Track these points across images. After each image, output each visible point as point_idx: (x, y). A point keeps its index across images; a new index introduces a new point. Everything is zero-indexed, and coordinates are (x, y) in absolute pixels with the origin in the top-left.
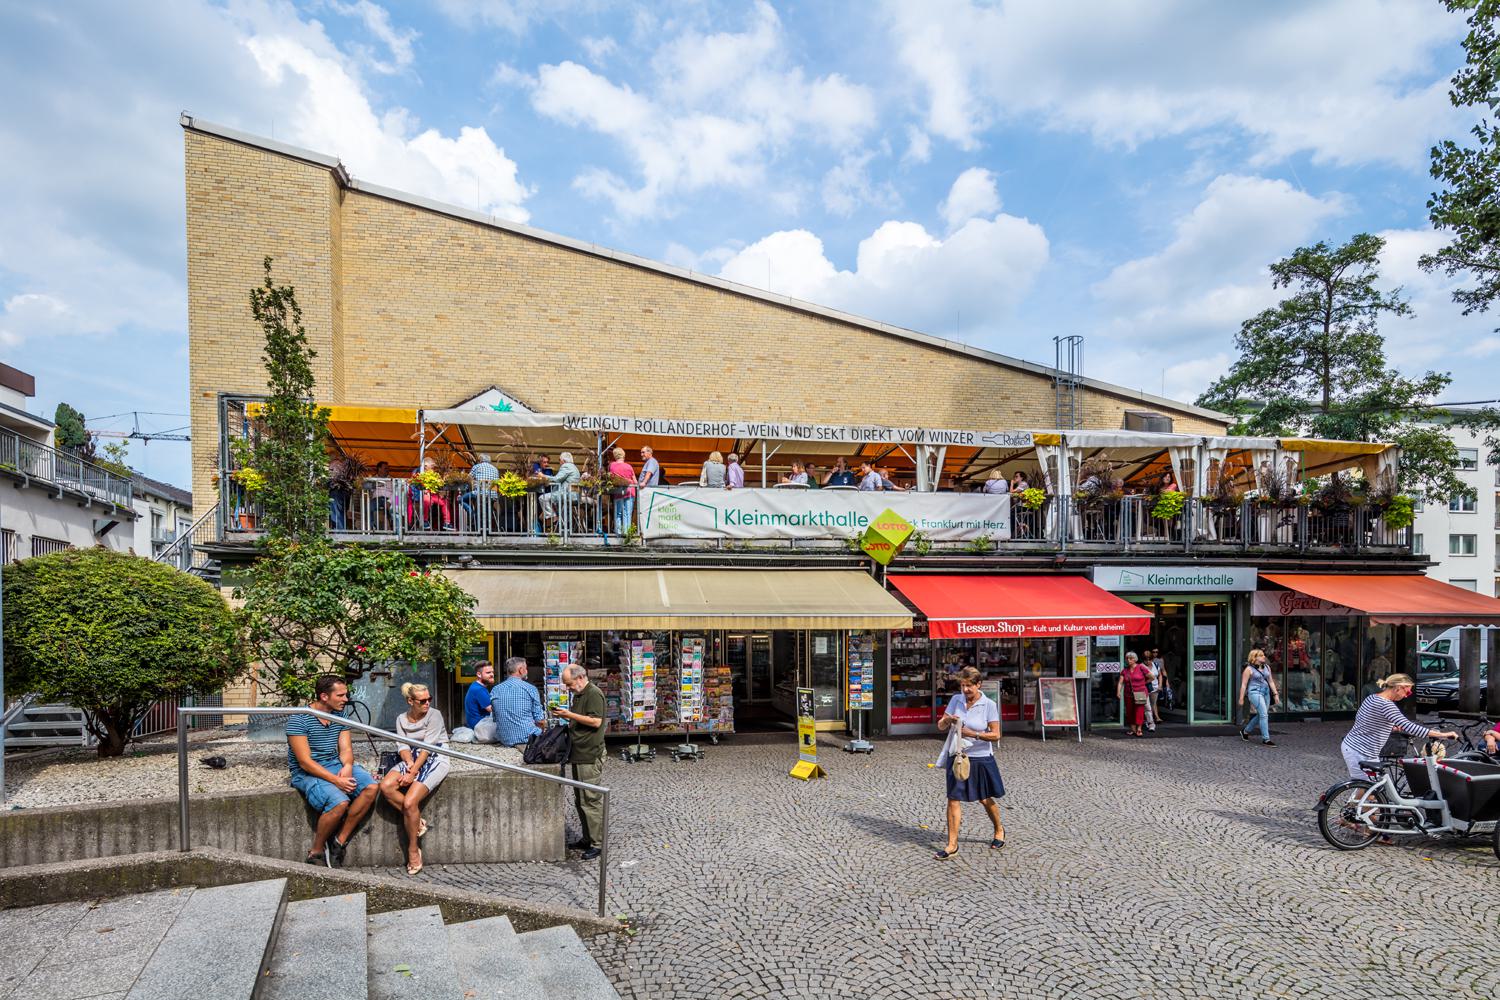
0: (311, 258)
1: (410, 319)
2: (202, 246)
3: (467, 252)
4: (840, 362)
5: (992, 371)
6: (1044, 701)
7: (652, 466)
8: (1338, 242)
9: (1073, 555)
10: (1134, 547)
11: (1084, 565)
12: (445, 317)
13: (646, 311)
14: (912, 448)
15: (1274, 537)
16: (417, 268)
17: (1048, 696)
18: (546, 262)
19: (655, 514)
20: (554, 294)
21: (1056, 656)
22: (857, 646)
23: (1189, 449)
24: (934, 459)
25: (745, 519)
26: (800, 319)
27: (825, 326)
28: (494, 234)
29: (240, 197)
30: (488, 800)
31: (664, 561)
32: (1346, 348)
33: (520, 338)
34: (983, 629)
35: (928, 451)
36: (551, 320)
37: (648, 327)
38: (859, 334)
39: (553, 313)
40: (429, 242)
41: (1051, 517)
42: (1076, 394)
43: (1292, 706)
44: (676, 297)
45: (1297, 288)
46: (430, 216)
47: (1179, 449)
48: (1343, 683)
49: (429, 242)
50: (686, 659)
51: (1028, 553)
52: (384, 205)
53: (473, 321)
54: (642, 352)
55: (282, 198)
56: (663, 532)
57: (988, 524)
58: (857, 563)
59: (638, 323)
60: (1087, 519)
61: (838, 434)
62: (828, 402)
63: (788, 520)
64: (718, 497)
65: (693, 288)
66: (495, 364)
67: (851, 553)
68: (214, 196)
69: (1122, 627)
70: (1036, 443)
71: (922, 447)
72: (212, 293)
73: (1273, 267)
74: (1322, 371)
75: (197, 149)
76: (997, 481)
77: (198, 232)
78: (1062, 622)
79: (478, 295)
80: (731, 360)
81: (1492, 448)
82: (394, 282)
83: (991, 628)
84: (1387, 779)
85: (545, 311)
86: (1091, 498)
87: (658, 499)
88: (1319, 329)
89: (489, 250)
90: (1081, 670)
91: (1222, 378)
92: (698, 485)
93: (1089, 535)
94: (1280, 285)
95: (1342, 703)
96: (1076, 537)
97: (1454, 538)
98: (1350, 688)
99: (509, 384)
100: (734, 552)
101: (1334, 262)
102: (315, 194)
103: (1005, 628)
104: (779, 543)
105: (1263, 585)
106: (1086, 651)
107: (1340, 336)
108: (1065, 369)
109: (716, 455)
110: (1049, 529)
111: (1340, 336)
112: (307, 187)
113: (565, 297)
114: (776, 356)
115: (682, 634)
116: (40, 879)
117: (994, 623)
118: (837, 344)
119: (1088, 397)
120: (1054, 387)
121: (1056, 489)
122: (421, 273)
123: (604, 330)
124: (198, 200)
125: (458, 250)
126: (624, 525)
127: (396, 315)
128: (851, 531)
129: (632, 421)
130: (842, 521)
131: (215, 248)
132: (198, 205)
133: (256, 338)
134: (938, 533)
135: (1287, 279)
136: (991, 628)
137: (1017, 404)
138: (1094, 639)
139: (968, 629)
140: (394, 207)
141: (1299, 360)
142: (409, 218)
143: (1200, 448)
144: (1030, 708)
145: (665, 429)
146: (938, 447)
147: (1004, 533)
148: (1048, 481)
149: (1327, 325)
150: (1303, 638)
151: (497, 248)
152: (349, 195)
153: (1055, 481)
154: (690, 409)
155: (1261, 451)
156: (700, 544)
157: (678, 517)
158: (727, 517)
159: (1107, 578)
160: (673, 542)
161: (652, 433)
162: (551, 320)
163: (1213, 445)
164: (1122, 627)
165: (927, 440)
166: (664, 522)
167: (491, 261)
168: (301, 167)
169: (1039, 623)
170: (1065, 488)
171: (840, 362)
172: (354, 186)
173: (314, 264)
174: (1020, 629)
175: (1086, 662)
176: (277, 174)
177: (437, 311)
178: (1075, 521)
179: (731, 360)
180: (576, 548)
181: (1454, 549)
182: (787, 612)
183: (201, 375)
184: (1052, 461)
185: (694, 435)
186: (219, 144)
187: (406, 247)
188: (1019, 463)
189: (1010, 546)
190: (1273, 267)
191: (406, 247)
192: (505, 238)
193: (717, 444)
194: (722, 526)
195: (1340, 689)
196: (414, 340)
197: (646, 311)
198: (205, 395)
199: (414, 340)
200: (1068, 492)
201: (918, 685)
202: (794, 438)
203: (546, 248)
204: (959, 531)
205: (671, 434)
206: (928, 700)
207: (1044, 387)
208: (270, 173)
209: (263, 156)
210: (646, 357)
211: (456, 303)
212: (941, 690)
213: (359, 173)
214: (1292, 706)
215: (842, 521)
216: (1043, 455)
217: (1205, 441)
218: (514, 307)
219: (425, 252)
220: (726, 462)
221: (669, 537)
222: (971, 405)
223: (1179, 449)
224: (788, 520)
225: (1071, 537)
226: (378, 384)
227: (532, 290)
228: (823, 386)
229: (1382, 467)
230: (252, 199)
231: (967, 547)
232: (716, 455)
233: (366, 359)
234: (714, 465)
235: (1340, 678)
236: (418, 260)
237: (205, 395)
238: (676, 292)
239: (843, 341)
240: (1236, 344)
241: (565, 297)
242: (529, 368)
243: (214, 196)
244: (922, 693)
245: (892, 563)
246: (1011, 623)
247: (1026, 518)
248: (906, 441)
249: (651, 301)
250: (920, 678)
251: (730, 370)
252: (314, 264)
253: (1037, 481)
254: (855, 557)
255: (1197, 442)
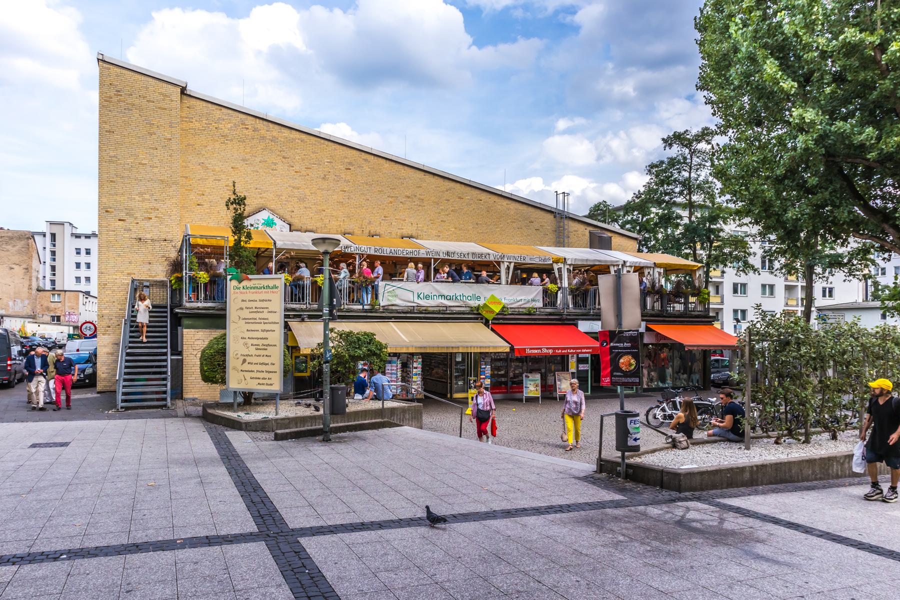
0: (169, 136)
1: (217, 169)
2: (107, 127)
3: (249, 133)
4: (448, 200)
5: (524, 207)
6: (558, 383)
7: (380, 270)
8: (695, 130)
9: (569, 315)
10: (595, 311)
11: (574, 320)
12: (238, 168)
13: (347, 169)
14: (499, 263)
15: (653, 307)
16: (222, 140)
17: (560, 380)
18: (294, 140)
19: (386, 294)
20: (297, 157)
21: (562, 362)
22: (484, 359)
23: (618, 265)
24: (508, 268)
25: (427, 297)
26: (428, 178)
27: (440, 180)
28: (265, 123)
29: (129, 101)
30: (404, 415)
31: (390, 318)
32: (699, 187)
33: (279, 181)
34: (536, 351)
35: (506, 264)
36: (296, 172)
37: (348, 178)
38: (458, 185)
39: (297, 168)
40: (229, 126)
41: (560, 295)
42: (566, 222)
43: (661, 385)
44: (363, 162)
45: (675, 151)
46: (230, 112)
47: (614, 266)
48: (683, 374)
49: (229, 126)
50: (415, 365)
51: (550, 314)
52: (204, 104)
53: (253, 171)
54: (345, 191)
55: (153, 102)
56: (390, 303)
57: (533, 300)
58: (477, 319)
59: (343, 176)
60: (574, 298)
61: (466, 256)
62: (442, 221)
63: (445, 297)
64: (413, 286)
65: (372, 157)
66: (264, 195)
67: (474, 314)
68: (115, 99)
69: (591, 350)
70: (553, 262)
71: (503, 262)
72: (112, 154)
73: (663, 139)
74: (688, 197)
75: (106, 72)
76: (536, 278)
77: (105, 119)
78: (567, 348)
79: (256, 156)
80: (392, 197)
81: (763, 250)
82: (209, 148)
83: (539, 351)
84: (665, 405)
85: (293, 167)
86: (577, 289)
87: (388, 287)
88: (686, 174)
89: (263, 132)
90: (573, 368)
91: (639, 191)
92: (402, 280)
93: (575, 304)
94: (667, 148)
95: (682, 383)
96: (571, 306)
97: (764, 286)
98: (685, 376)
99: (272, 207)
100: (422, 313)
101: (693, 140)
102: (172, 101)
103: (545, 351)
104: (441, 309)
105: (648, 329)
106: (575, 359)
107: (697, 180)
108: (561, 209)
109: (412, 265)
110: (559, 302)
111: (697, 180)
112: (166, 96)
113: (304, 160)
114: (415, 196)
115: (412, 354)
116: (364, 424)
117: (541, 349)
118: (447, 191)
119: (571, 223)
120: (555, 217)
121: (561, 283)
122: (224, 143)
123: (324, 178)
124: (106, 101)
125: (245, 131)
126: (368, 299)
127: (210, 166)
128: (474, 303)
129: (373, 248)
130: (469, 298)
131: (115, 128)
132: (106, 104)
133: (228, 216)
134: (512, 304)
135: (671, 145)
136: (539, 351)
137: (536, 225)
138: (578, 355)
139: (530, 352)
140: (210, 105)
141: (677, 190)
142: (218, 112)
143: (622, 265)
144: (551, 386)
145: (388, 252)
146: (510, 263)
147: (540, 304)
148: (559, 281)
149: (690, 173)
150: (665, 354)
151: (267, 131)
152: (185, 97)
153: (561, 280)
154: (370, 223)
155: (648, 267)
156: (406, 309)
157: (396, 296)
158: (418, 296)
159: (584, 326)
160: (394, 308)
161: (382, 254)
162: (296, 172)
163: (628, 264)
164: (591, 350)
165: (506, 260)
166: (390, 298)
167: (263, 138)
168: (165, 85)
169: (558, 349)
170: (565, 284)
171: (448, 200)
172: (188, 93)
173: (170, 139)
174: (551, 351)
175: (575, 365)
176: (151, 89)
177: (233, 165)
178: (570, 298)
179: (392, 197)
180: (351, 311)
181: (764, 293)
182: (459, 344)
183: (104, 200)
184: (560, 270)
185: (401, 255)
186: (118, 70)
187: (216, 128)
188: (546, 271)
189: (542, 310)
190: (663, 139)
191: (216, 128)
192: (271, 125)
193: (412, 260)
194: (416, 300)
195: (681, 377)
196: (219, 180)
197: (347, 169)
198: (107, 211)
199: (219, 180)
200: (567, 285)
201: (502, 376)
202: (446, 257)
203: (294, 132)
204: (520, 303)
205: (391, 255)
206: (506, 383)
207: (550, 217)
208: (147, 88)
209: (143, 78)
210: (346, 194)
211: (244, 160)
212: (511, 378)
213: (192, 89)
214: (661, 385)
215: (469, 298)
216: (556, 267)
217: (624, 262)
218: (275, 164)
219: (226, 131)
220: (416, 268)
221: (393, 305)
222: (514, 225)
223: (614, 266)
224: (445, 297)
225: (568, 306)
226: (198, 205)
227: (286, 155)
228: (440, 213)
229: (697, 275)
230: (137, 102)
231: (524, 310)
232: (412, 265)
233: (192, 190)
234: (411, 269)
235: (682, 371)
236: (222, 136)
237: (107, 211)
238: (364, 159)
239: (450, 189)
240: (646, 172)
241: (304, 160)
242: (283, 198)
243: (115, 99)
244: (503, 379)
245: (494, 319)
246: (547, 349)
247: (549, 296)
248: (496, 260)
249: (350, 163)
250: (503, 372)
251: (391, 202)
252: (170, 139)
253: (554, 281)
254: (475, 315)
255: (621, 263)
